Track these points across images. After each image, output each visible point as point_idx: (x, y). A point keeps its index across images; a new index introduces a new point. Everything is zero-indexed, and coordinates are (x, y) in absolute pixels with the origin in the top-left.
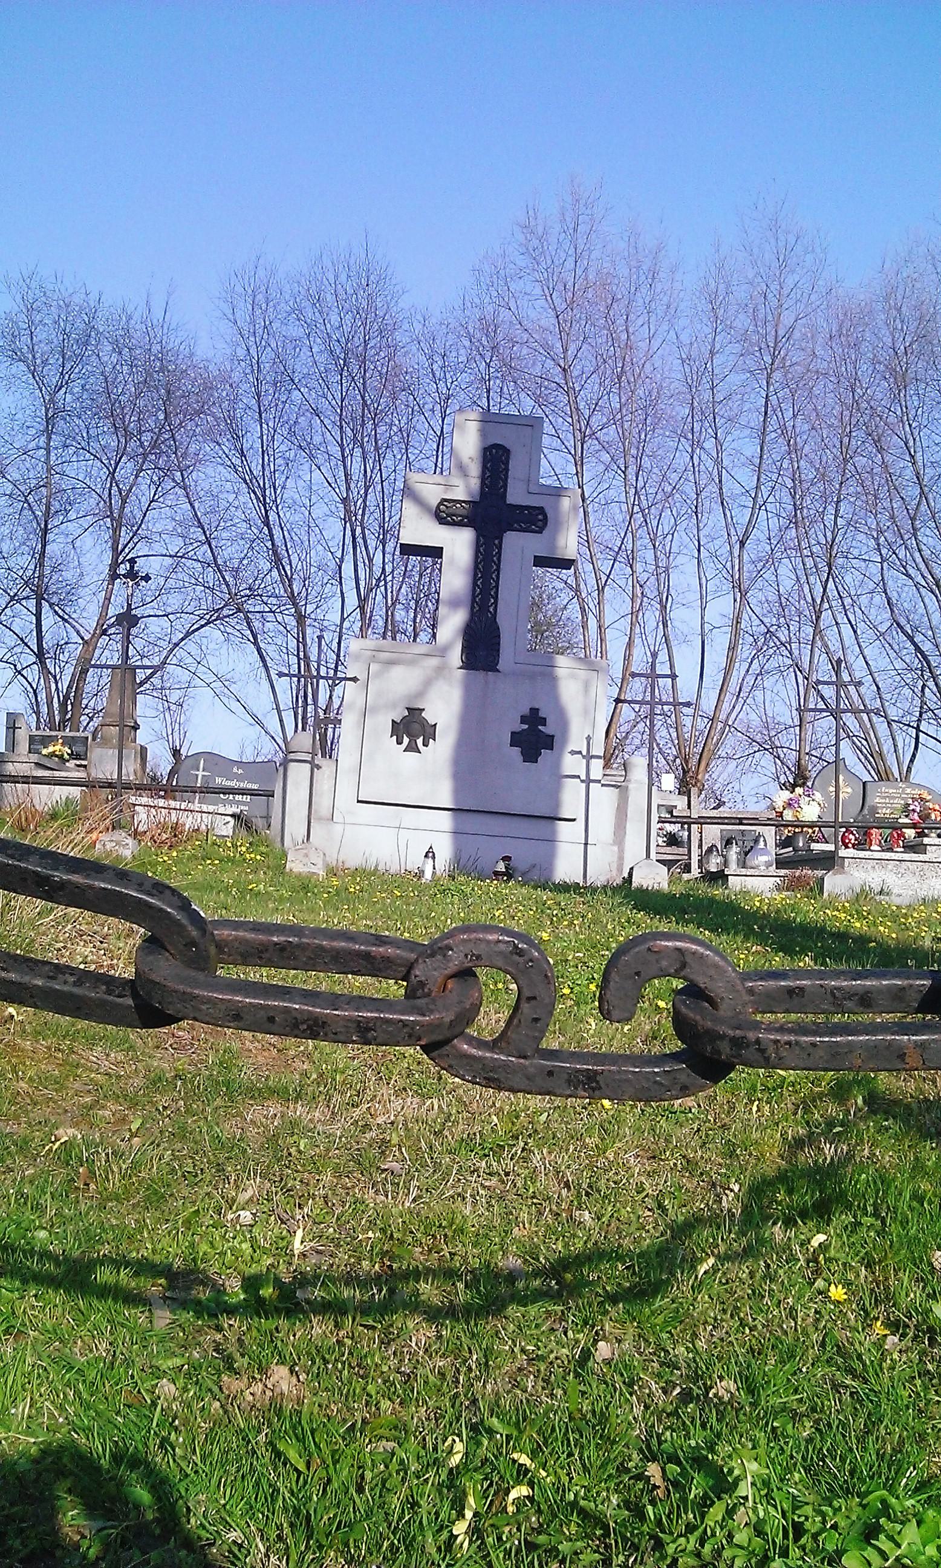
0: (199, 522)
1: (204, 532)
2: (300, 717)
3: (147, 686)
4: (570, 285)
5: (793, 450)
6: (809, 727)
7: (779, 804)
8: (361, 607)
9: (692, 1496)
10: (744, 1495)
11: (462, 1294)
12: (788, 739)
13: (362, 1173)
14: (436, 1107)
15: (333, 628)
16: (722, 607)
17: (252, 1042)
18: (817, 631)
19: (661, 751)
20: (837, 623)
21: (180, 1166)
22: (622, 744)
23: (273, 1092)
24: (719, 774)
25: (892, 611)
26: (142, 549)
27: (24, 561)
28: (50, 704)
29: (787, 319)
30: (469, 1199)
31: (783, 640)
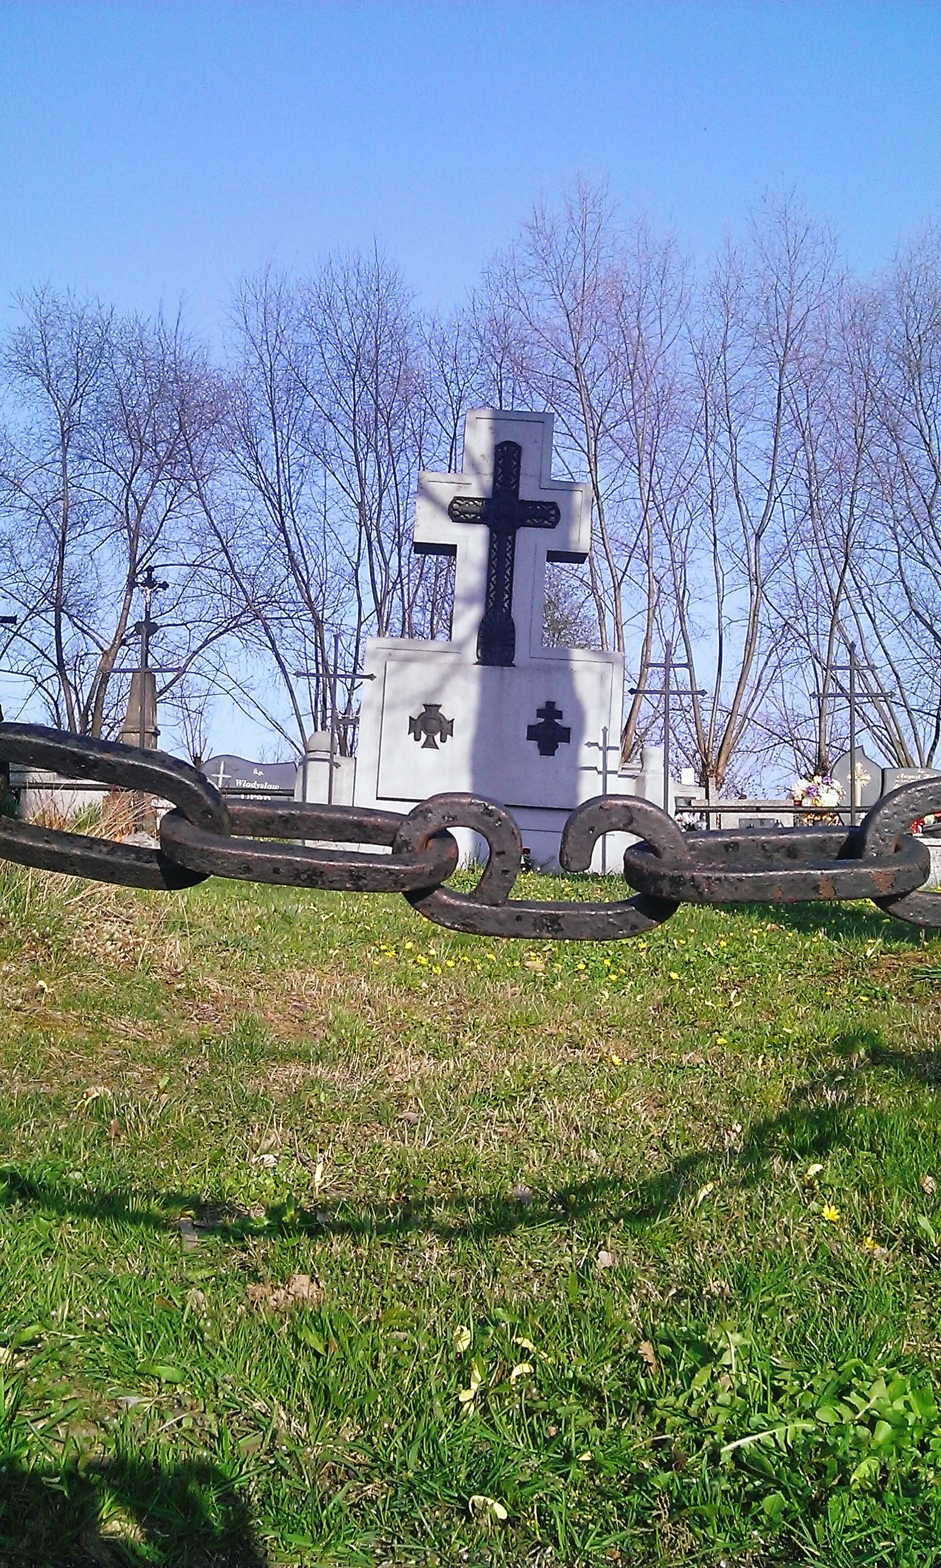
0: (216, 530)
1: (221, 541)
2: (319, 722)
3: (166, 694)
4: (580, 283)
5: (808, 441)
6: (829, 719)
7: (798, 794)
8: (379, 611)
9: (681, 1369)
10: (728, 1363)
11: (473, 1216)
12: (808, 732)
13: (380, 1123)
14: (452, 1067)
15: (350, 632)
16: (739, 600)
17: (274, 1013)
18: (835, 621)
19: (680, 746)
20: (855, 614)
21: (207, 1119)
22: (641, 738)
23: (294, 1055)
24: (740, 767)
25: (910, 600)
26: (159, 559)
27: (43, 574)
28: (71, 715)
29: (798, 311)
30: (482, 1142)
31: (802, 632)
